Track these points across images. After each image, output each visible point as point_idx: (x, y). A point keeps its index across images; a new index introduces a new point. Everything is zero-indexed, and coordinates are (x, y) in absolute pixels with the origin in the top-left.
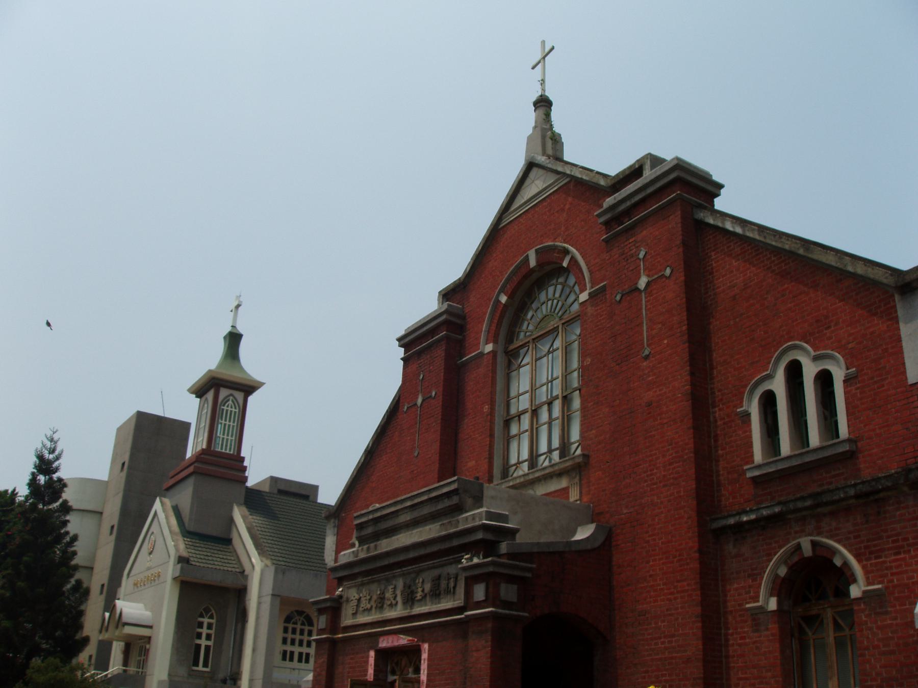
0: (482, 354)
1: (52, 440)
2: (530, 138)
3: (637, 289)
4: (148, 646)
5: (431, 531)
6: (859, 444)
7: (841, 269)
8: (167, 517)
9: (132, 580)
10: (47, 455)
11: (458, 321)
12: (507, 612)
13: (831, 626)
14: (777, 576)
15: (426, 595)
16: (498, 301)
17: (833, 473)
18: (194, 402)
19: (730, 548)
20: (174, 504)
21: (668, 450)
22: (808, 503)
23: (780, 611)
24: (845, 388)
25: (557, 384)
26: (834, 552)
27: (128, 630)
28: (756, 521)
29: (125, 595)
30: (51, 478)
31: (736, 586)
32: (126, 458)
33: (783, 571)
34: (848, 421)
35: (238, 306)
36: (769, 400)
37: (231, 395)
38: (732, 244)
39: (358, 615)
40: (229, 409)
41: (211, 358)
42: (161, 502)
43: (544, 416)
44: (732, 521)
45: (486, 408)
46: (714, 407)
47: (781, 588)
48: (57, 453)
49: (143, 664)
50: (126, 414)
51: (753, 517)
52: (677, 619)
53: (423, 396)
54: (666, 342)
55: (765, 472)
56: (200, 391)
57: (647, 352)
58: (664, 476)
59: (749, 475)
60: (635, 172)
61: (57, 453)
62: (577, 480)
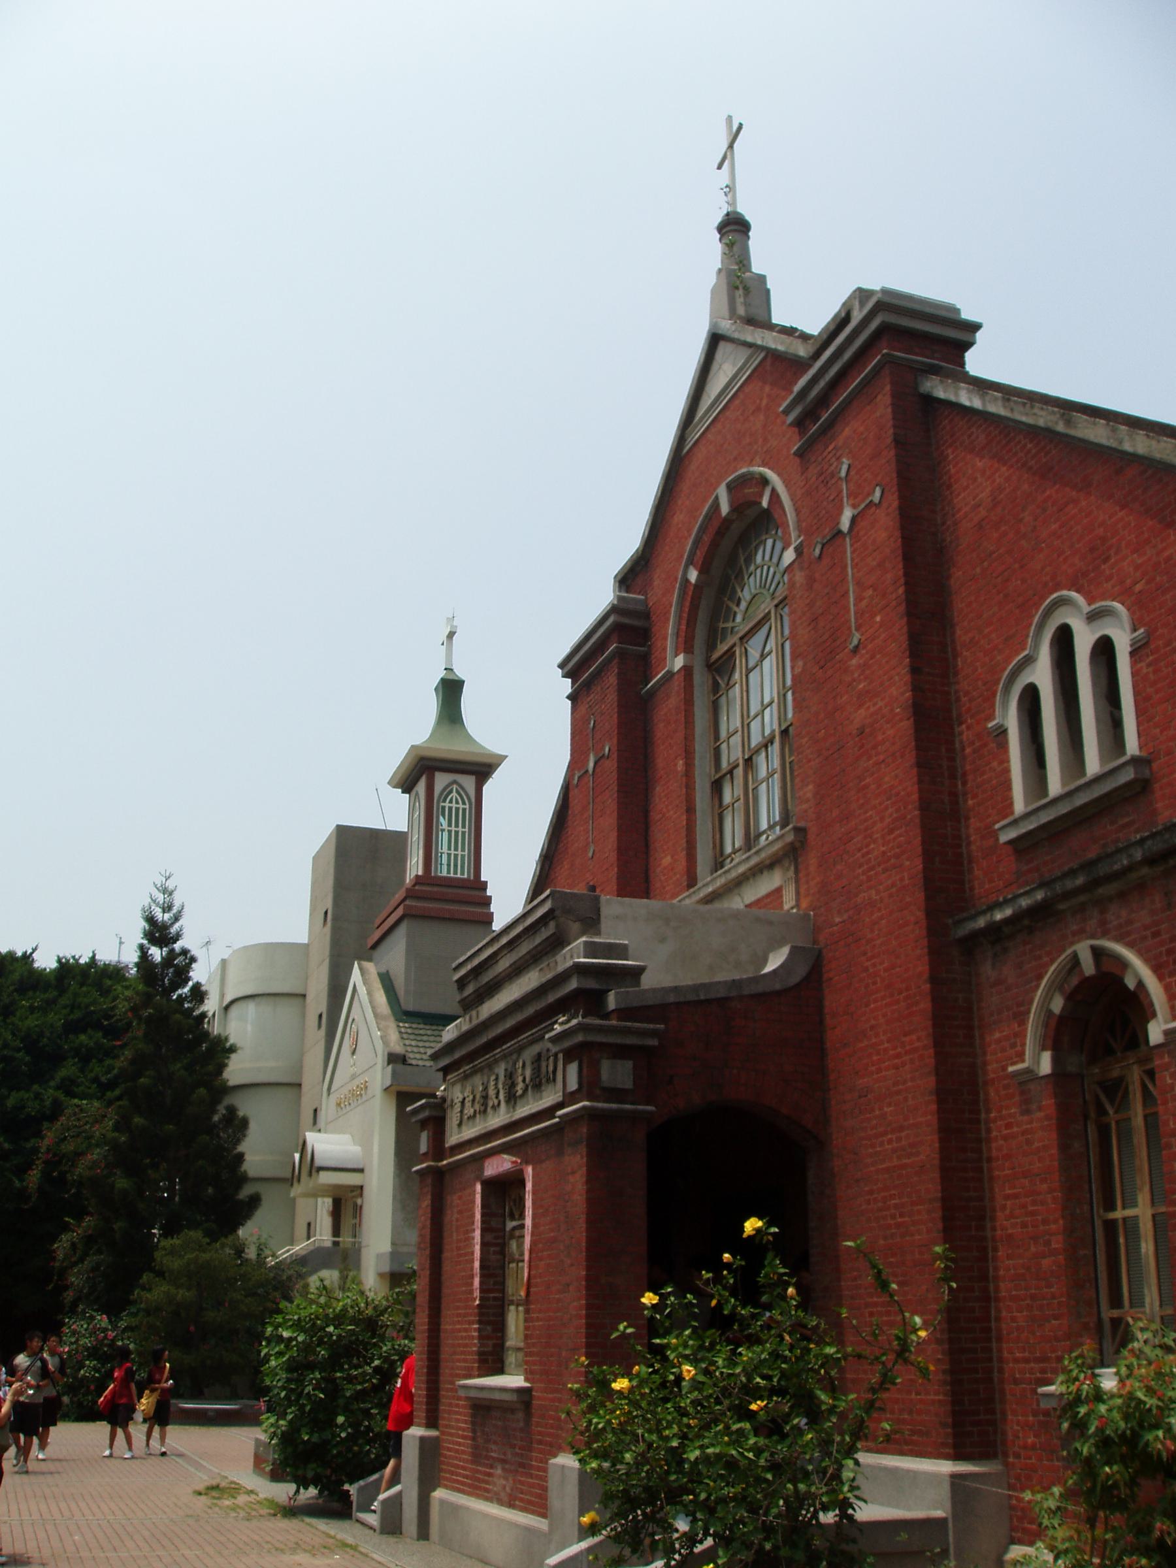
0: (670, 675)
2: (714, 292)
3: (840, 532)
4: (359, 1201)
5: (531, 980)
6: (1155, 765)
8: (370, 994)
9: (334, 1098)
12: (614, 1106)
14: (1050, 1013)
15: (527, 1086)
16: (686, 581)
17: (1121, 822)
18: (402, 800)
19: (988, 971)
20: (383, 970)
21: (887, 808)
22: (1080, 881)
23: (1059, 1074)
24: (1133, 664)
26: (1124, 965)
27: (325, 1178)
29: (327, 1124)
31: (997, 1035)
32: (329, 903)
33: (1057, 1004)
35: (451, 635)
37: (455, 782)
38: (974, 429)
39: (464, 1127)
40: (454, 805)
41: (418, 726)
42: (361, 969)
44: (981, 922)
46: (961, 724)
47: (1058, 1035)
49: (356, 1231)
50: (323, 833)
51: (1008, 912)
52: (906, 1099)
53: (596, 755)
54: (878, 619)
55: (1024, 831)
56: (406, 783)
58: (884, 853)
59: (1004, 838)
62: (791, 873)
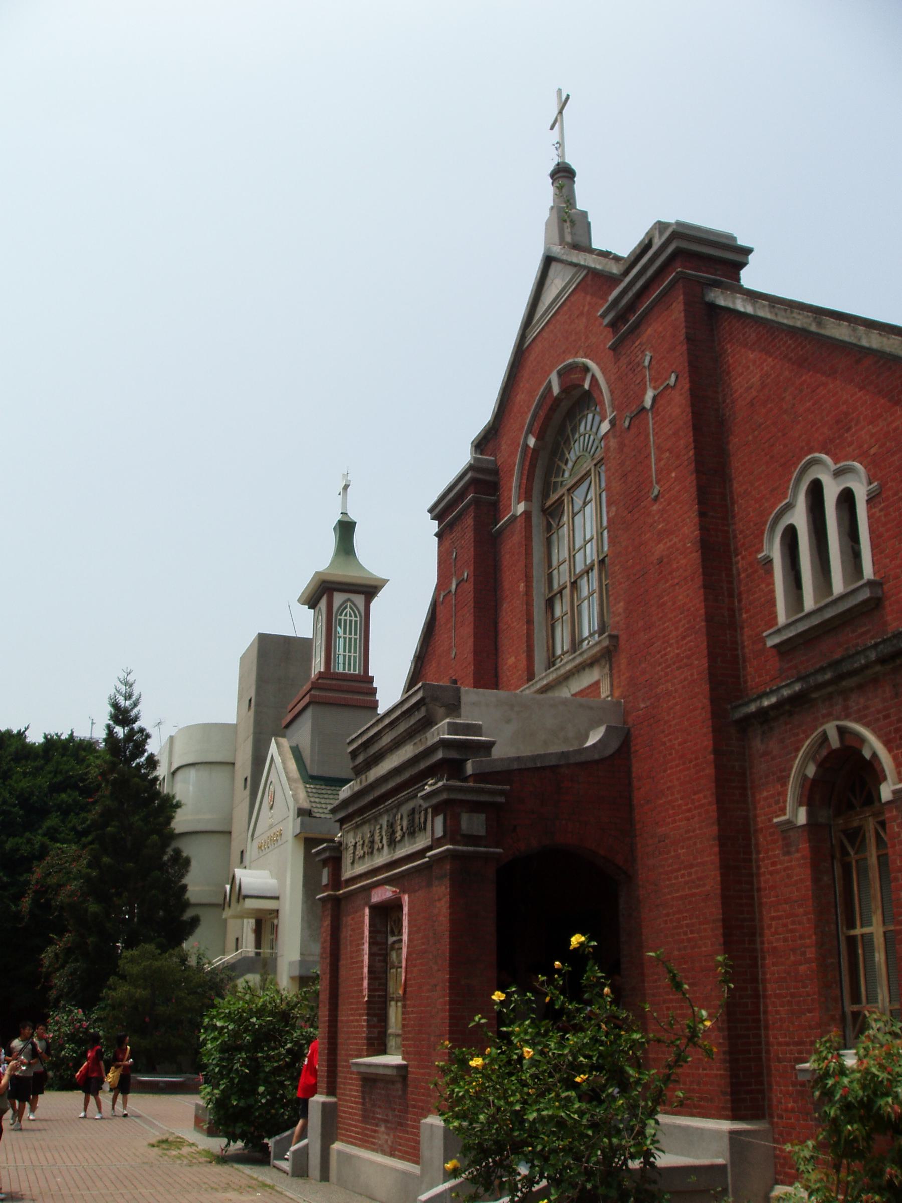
0: (514, 518)
1: (126, 683)
2: (548, 224)
3: (644, 408)
4: (275, 922)
5: (407, 752)
6: (886, 587)
7: (855, 345)
9: (256, 843)
10: (122, 702)
11: (488, 478)
12: (471, 848)
13: (873, 841)
14: (805, 777)
15: (404, 833)
16: (526, 446)
17: (860, 631)
18: (309, 613)
19: (758, 745)
20: (294, 745)
22: (828, 676)
23: (812, 824)
24: (869, 509)
26: (862, 740)
27: (250, 904)
29: (250, 862)
30: (132, 729)
31: (765, 794)
32: (252, 693)
33: (811, 771)
34: (873, 556)
35: (346, 487)
38: (747, 329)
39: (356, 865)
40: (348, 618)
41: (320, 557)
42: (277, 743)
44: (753, 708)
46: (737, 555)
47: (812, 794)
48: (134, 698)
49: (273, 944)
50: (248, 639)
51: (773, 700)
52: (695, 844)
53: (457, 579)
54: (673, 475)
55: (785, 637)
56: (312, 601)
57: (656, 492)
58: (678, 654)
59: (770, 643)
61: (134, 698)
62: (607, 670)
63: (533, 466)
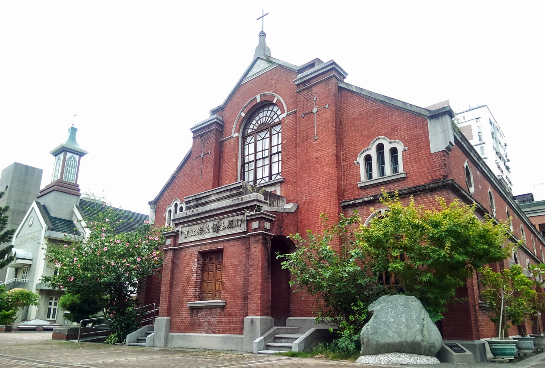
6: (408, 175)
25: (267, 152)
28: (362, 202)
36: (368, 159)
43: (260, 163)
44: (351, 202)
45: (234, 160)
50: (8, 162)
59: (359, 186)
60: (311, 65)
63: (242, 122)
